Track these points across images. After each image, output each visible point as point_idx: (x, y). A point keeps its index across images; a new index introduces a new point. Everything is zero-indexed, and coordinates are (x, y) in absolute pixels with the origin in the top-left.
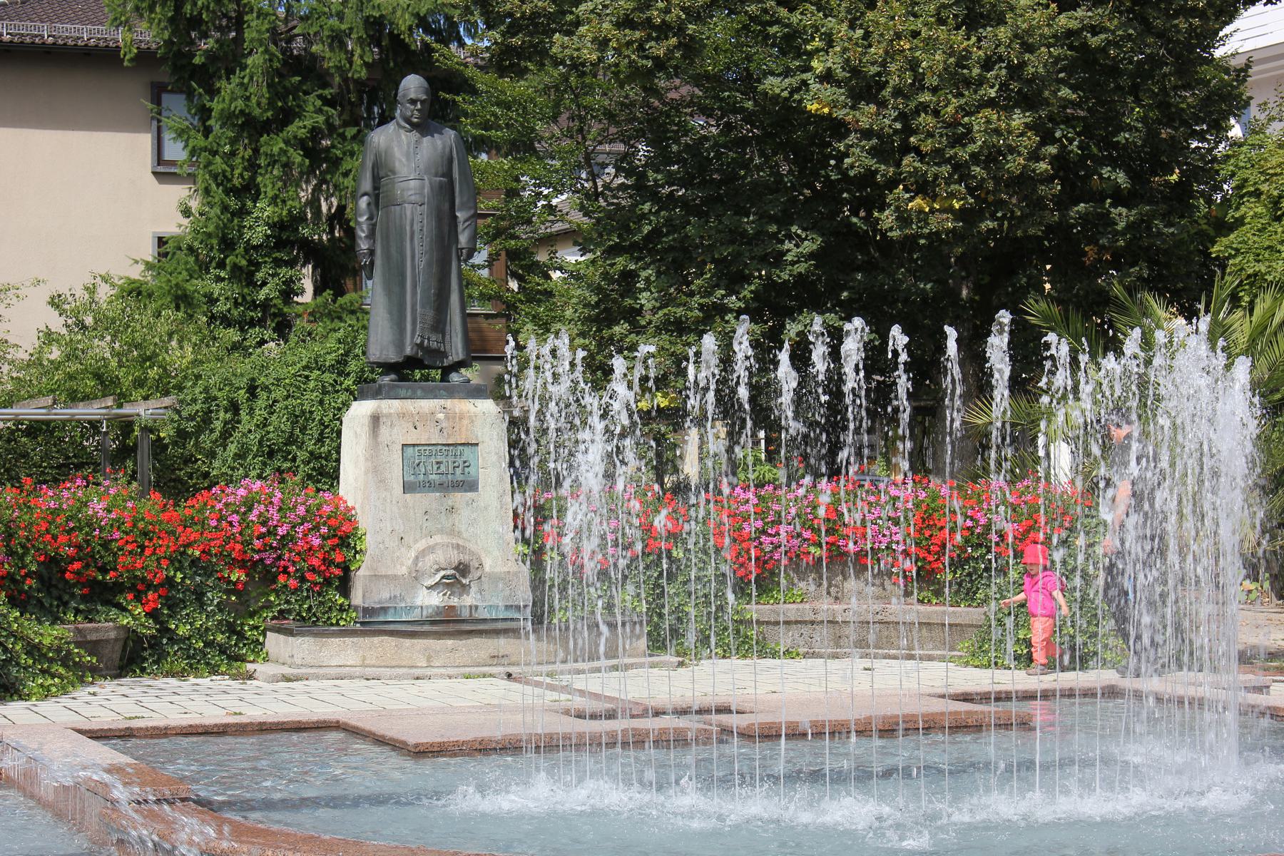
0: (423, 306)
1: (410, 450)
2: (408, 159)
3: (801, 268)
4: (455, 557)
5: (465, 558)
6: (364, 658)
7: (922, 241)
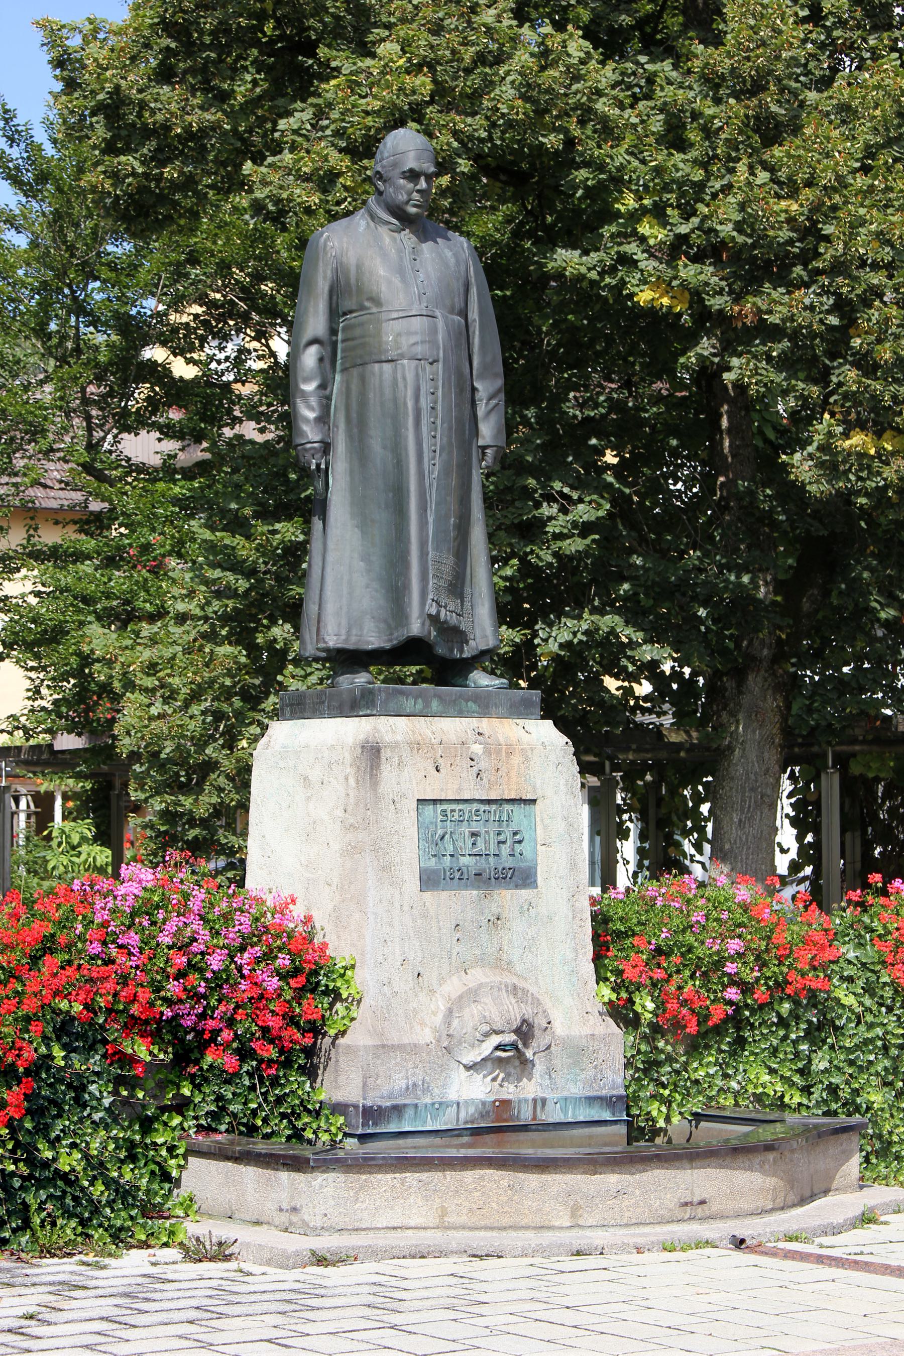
0: (437, 548)
1: (429, 809)
2: (404, 280)
3: (574, 545)
4: (515, 1012)
5: (528, 1011)
6: (444, 1212)
7: (862, 500)
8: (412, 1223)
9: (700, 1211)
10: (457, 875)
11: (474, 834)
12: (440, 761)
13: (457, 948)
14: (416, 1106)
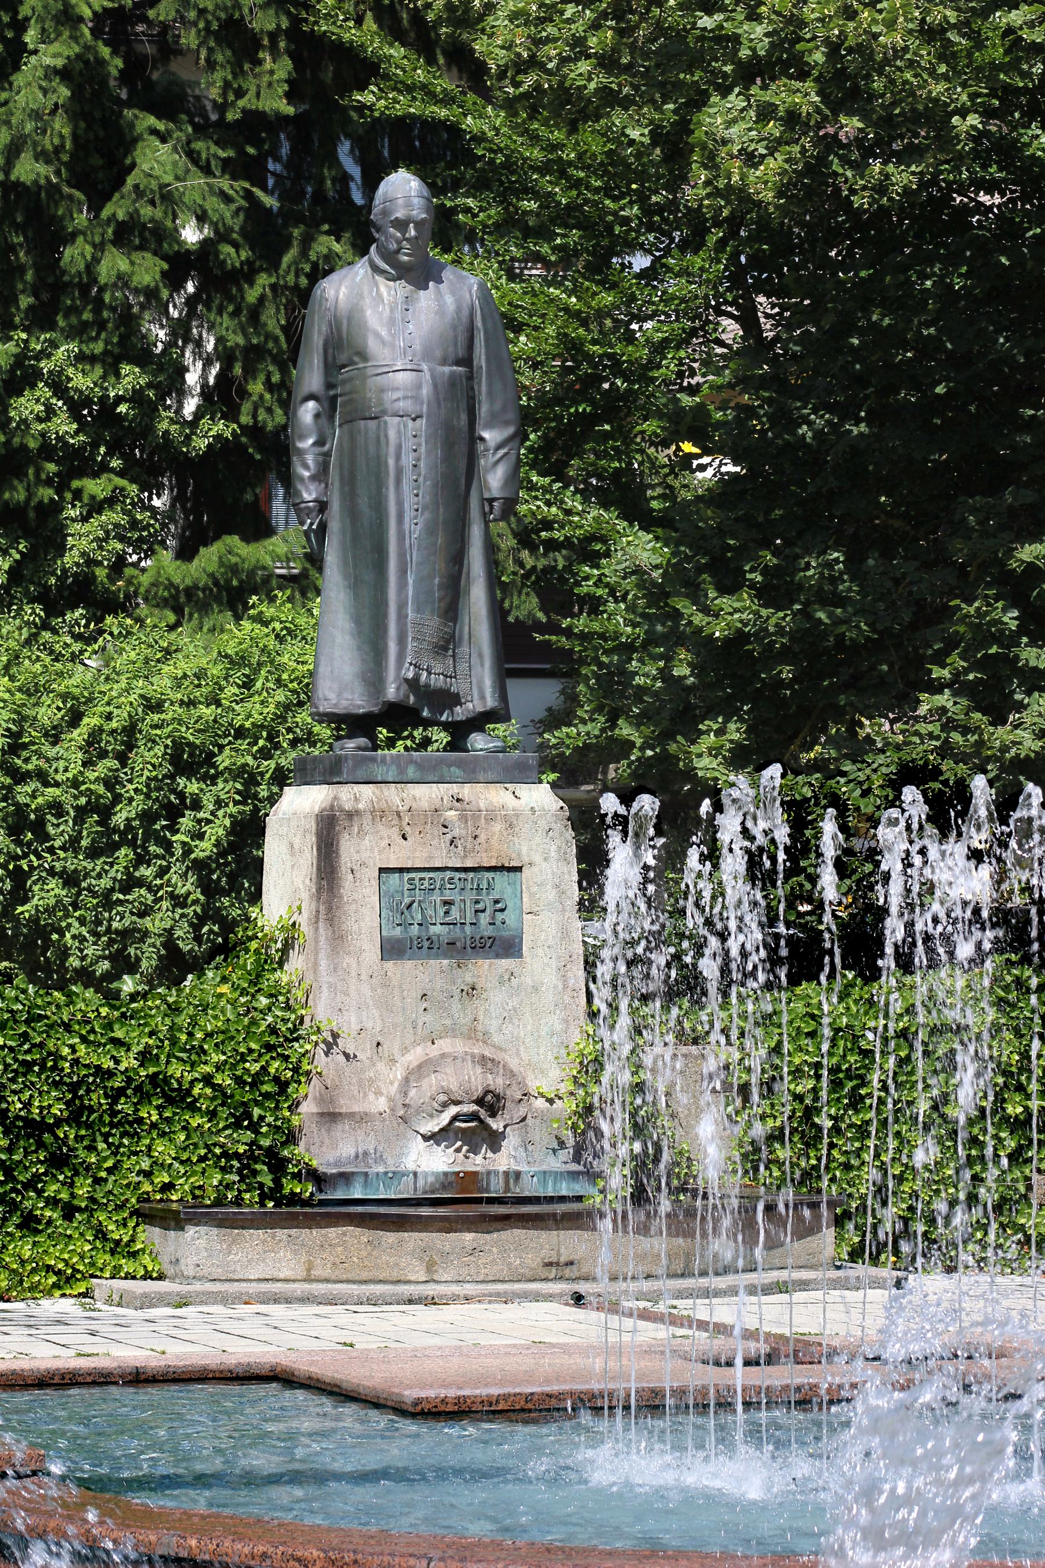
0: (418, 610)
4: (477, 1080)
5: (497, 1082)
8: (282, 1276)
9: (567, 1272)
10: (426, 944)
11: (445, 903)
12: (408, 829)
13: (428, 1018)
14: (366, 1174)
